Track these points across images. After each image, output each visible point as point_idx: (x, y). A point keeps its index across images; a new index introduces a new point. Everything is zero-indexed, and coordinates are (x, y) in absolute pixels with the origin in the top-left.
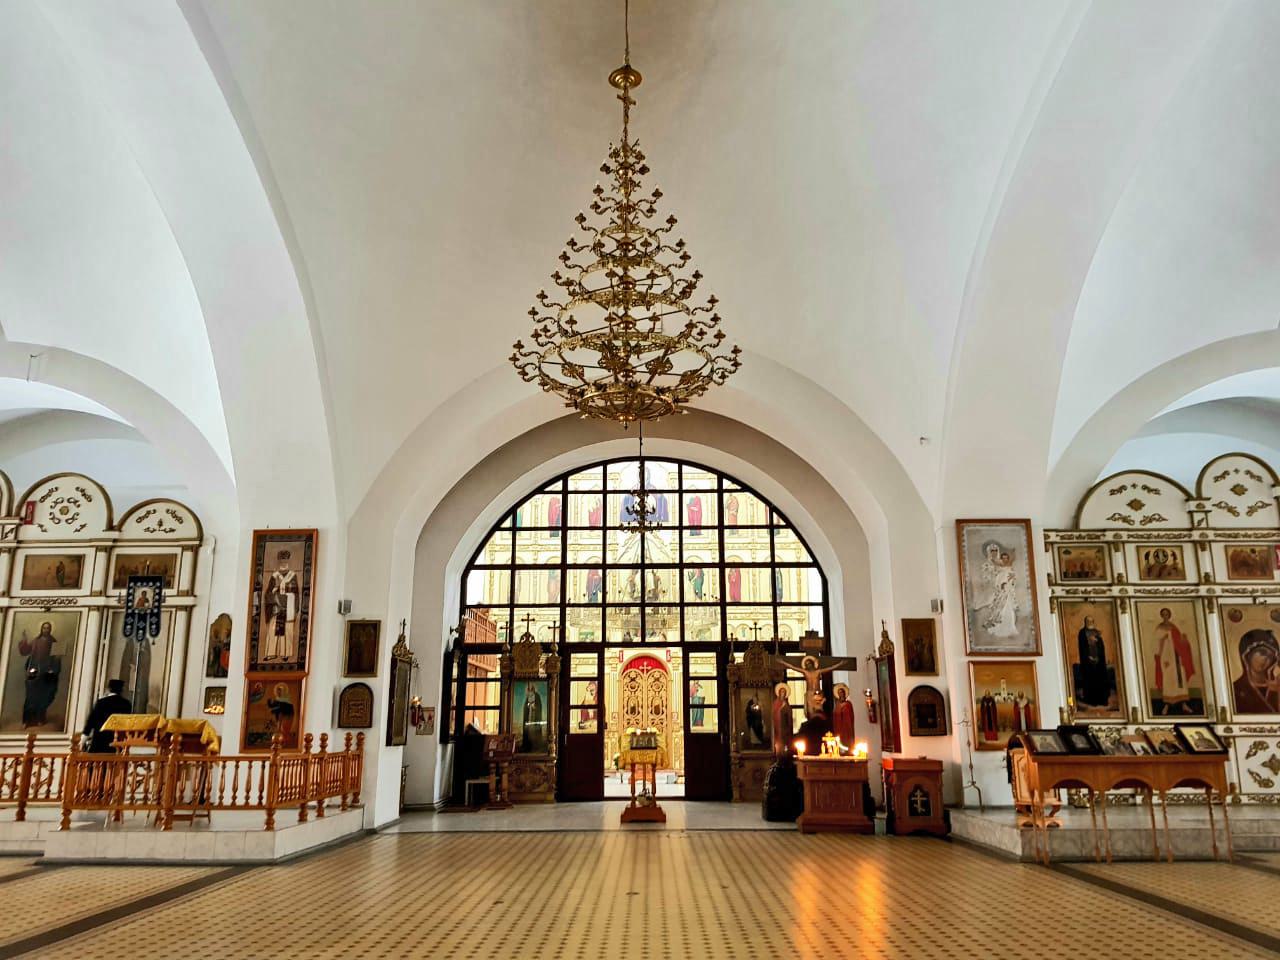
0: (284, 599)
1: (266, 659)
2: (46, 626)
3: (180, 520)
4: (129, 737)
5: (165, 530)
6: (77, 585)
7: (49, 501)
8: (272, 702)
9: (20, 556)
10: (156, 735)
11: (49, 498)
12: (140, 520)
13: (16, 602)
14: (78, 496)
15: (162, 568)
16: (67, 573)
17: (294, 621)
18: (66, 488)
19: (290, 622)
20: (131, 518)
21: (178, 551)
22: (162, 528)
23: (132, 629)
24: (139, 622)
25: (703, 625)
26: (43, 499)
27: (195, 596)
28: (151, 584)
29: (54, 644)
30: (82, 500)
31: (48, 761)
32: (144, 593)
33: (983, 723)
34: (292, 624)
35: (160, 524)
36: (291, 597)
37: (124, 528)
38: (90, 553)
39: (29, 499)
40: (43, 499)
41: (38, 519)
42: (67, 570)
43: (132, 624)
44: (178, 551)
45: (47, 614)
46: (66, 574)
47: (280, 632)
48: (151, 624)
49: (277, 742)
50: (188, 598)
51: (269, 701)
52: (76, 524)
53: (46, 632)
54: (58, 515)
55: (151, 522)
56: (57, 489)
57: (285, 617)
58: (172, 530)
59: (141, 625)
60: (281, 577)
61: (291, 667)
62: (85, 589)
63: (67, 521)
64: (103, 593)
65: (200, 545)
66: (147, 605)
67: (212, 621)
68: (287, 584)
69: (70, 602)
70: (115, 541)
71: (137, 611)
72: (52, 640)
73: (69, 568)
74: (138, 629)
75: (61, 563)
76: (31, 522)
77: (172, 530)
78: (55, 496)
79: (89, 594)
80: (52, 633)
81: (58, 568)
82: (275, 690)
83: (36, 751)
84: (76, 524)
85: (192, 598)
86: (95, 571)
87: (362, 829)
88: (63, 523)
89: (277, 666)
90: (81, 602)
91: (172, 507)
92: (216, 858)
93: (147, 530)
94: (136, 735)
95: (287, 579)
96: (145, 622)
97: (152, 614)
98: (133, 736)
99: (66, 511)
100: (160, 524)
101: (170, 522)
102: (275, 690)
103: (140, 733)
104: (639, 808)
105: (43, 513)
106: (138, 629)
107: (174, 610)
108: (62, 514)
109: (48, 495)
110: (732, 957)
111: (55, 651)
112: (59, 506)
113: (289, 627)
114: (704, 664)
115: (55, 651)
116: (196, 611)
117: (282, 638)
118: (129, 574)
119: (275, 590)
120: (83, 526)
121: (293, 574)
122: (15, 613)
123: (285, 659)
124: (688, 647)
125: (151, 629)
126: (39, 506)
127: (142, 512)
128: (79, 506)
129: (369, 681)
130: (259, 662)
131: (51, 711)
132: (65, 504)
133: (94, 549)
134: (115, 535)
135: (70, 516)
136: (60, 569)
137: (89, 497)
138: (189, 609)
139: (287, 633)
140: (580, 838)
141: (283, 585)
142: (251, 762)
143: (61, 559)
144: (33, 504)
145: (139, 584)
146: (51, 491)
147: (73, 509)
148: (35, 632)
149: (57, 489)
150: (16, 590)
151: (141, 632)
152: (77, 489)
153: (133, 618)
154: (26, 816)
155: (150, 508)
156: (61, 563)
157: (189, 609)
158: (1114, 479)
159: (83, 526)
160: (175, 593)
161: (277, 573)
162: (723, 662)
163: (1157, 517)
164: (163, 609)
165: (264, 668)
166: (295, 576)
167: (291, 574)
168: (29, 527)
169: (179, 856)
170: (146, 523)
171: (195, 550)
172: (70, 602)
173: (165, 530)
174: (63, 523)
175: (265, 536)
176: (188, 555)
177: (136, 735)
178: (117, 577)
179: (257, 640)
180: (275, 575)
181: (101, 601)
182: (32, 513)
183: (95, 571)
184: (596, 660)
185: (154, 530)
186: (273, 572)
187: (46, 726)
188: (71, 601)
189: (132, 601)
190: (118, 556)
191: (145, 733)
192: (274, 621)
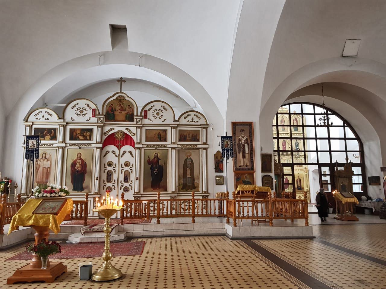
0: (244, 146)
1: (240, 166)
2: (156, 154)
3: (51, 115)
4: (245, 193)
5: (194, 122)
6: (165, 140)
7: (152, 111)
8: (244, 181)
9: (69, 127)
10: (254, 192)
11: (151, 109)
12: (185, 118)
13: (145, 146)
14: (162, 109)
15: (195, 135)
16: (162, 136)
17: (248, 154)
18: (158, 106)
19: (247, 154)
20: (182, 116)
21: (58, 127)
22: (44, 118)
23: (29, 156)
24: (226, 152)
25: (324, 158)
26: (149, 110)
27: (208, 145)
28: (229, 139)
29: (348, 160)
30: (164, 111)
31: (196, 201)
32: (227, 142)
33: (75, 201)
34: (248, 154)
35: (193, 119)
36: (246, 145)
37: (180, 121)
38: (95, 128)
39: (144, 109)
40: (149, 110)
41: (148, 117)
42: (162, 135)
43: (29, 154)
44: (58, 127)
45: (80, 150)
46: (162, 136)
47: (244, 157)
48: (36, 154)
49: (284, 196)
50: (62, 144)
51: (243, 180)
52: (163, 119)
53: (156, 157)
54: (156, 115)
55: (189, 118)
56: (154, 106)
57: (245, 152)
58: (197, 122)
59: (32, 154)
60: (242, 138)
61: (249, 169)
62: (94, 141)
63: (159, 117)
64: (174, 143)
65: (208, 127)
66: (228, 146)
67: (215, 153)
68: (244, 141)
69: (88, 145)
70: (178, 125)
71: (225, 149)
72: (159, 159)
73: (162, 134)
74: (31, 156)
75: (159, 132)
76: (146, 118)
77: (197, 122)
78: (153, 109)
79: (171, 143)
80: (158, 157)
81: (158, 134)
82: (245, 177)
83: (161, 198)
84: (163, 119)
85: (207, 145)
86: (172, 136)
87: (28, 238)
88: (158, 118)
89: (244, 169)
90: (93, 145)
91: (196, 114)
92: (293, 236)
93: (188, 121)
94: (247, 192)
95: (244, 139)
96: (229, 152)
97: (231, 150)
98: (247, 193)
99: (158, 114)
100: (193, 119)
101: (196, 119)
102: (245, 177)
103: (249, 191)
104: (38, 232)
105: (150, 114)
106: (31, 156)
107: (57, 149)
108: (157, 115)
109: (151, 108)
110: (175, 287)
111: (161, 163)
112: (156, 112)
113: (247, 156)
114: (326, 170)
115: (161, 163)
116: (209, 150)
117: (245, 159)
118: (183, 137)
119: (240, 143)
120: (165, 120)
121: (246, 138)
122: (68, 149)
123: (247, 166)
124: (321, 165)
125: (231, 155)
126: (148, 112)
127: (186, 115)
128: (163, 112)
129: (270, 174)
130: (238, 167)
131: (161, 184)
132: (158, 111)
133: (97, 126)
134: (177, 123)
135: (160, 116)
136: (159, 135)
137: (91, 107)
138: (206, 149)
139: (246, 157)
140: (149, 240)
141: (243, 141)
142: (248, 202)
143: (159, 131)
144: (146, 111)
145: (225, 139)
146: (75, 105)
147: (161, 114)
148: (152, 157)
149: (154, 106)
150: (68, 140)
151: (228, 156)
152: (86, 104)
153: (29, 152)
154: (195, 222)
155: (189, 113)
156: (159, 132)
157: (206, 149)
158: (91, 102)
159: (165, 120)
160: (201, 143)
161: (241, 137)
162: (332, 170)
163: (83, 115)
164: (40, 148)
165: (240, 169)
166: (247, 138)
167: (246, 137)
168: (145, 119)
169: (280, 235)
170: (187, 119)
171: (206, 128)
172: (88, 145)
173: (194, 122)
174: (158, 118)
175: (235, 124)
176: (62, 128)
177: (247, 192)
178: (180, 138)
179: (251, 159)
180: (240, 137)
181: (175, 146)
182: (146, 114)
183: (172, 136)
184: (291, 170)
185: (40, 119)
186: (239, 136)
187: (160, 189)
188: (89, 145)
189: (224, 145)
190: (71, 129)
191: (251, 191)
192: (241, 153)
